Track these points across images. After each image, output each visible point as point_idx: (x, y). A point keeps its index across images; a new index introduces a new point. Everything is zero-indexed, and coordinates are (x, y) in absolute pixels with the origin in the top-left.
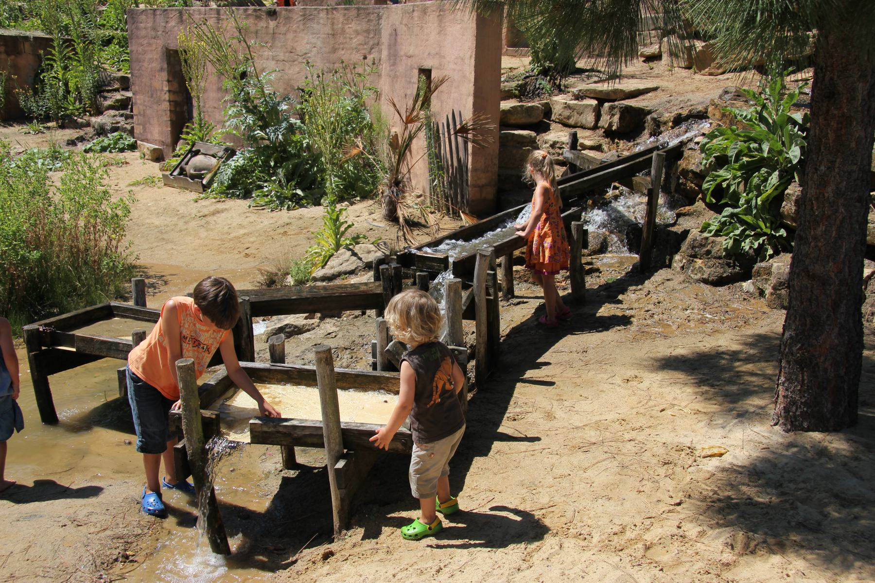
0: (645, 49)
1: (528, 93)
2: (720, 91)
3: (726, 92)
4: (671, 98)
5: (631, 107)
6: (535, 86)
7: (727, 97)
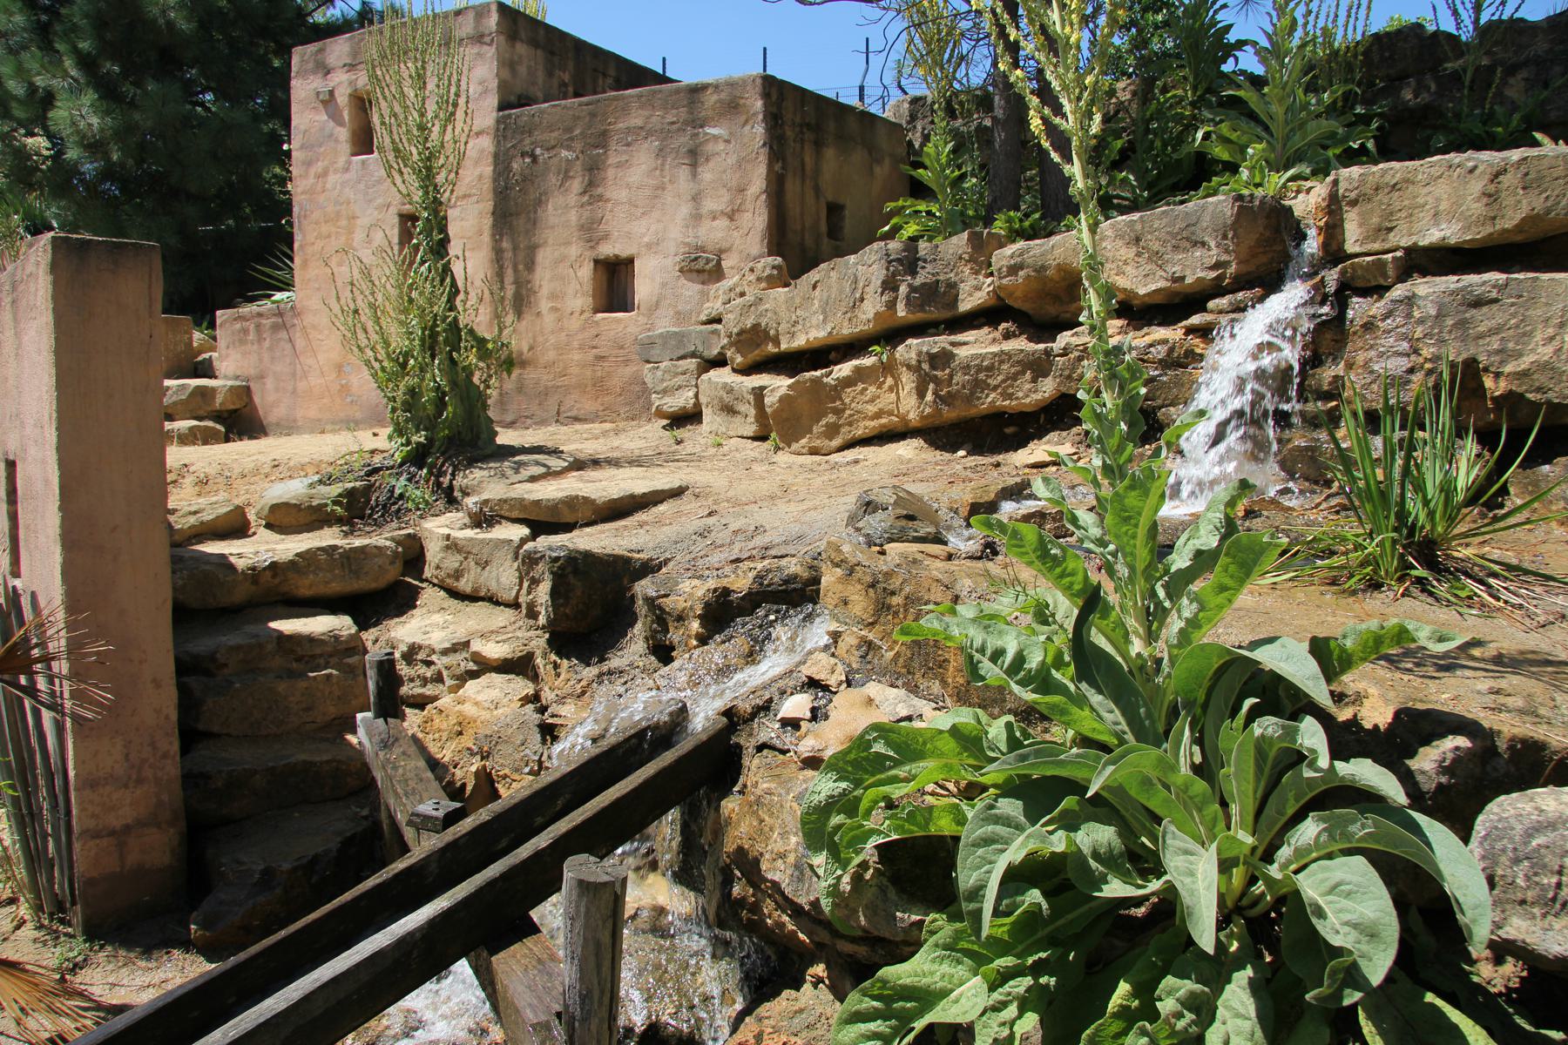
2: (850, 501)
3: (869, 506)
4: (711, 521)
5: (588, 555)
6: (392, 491)
7: (876, 523)
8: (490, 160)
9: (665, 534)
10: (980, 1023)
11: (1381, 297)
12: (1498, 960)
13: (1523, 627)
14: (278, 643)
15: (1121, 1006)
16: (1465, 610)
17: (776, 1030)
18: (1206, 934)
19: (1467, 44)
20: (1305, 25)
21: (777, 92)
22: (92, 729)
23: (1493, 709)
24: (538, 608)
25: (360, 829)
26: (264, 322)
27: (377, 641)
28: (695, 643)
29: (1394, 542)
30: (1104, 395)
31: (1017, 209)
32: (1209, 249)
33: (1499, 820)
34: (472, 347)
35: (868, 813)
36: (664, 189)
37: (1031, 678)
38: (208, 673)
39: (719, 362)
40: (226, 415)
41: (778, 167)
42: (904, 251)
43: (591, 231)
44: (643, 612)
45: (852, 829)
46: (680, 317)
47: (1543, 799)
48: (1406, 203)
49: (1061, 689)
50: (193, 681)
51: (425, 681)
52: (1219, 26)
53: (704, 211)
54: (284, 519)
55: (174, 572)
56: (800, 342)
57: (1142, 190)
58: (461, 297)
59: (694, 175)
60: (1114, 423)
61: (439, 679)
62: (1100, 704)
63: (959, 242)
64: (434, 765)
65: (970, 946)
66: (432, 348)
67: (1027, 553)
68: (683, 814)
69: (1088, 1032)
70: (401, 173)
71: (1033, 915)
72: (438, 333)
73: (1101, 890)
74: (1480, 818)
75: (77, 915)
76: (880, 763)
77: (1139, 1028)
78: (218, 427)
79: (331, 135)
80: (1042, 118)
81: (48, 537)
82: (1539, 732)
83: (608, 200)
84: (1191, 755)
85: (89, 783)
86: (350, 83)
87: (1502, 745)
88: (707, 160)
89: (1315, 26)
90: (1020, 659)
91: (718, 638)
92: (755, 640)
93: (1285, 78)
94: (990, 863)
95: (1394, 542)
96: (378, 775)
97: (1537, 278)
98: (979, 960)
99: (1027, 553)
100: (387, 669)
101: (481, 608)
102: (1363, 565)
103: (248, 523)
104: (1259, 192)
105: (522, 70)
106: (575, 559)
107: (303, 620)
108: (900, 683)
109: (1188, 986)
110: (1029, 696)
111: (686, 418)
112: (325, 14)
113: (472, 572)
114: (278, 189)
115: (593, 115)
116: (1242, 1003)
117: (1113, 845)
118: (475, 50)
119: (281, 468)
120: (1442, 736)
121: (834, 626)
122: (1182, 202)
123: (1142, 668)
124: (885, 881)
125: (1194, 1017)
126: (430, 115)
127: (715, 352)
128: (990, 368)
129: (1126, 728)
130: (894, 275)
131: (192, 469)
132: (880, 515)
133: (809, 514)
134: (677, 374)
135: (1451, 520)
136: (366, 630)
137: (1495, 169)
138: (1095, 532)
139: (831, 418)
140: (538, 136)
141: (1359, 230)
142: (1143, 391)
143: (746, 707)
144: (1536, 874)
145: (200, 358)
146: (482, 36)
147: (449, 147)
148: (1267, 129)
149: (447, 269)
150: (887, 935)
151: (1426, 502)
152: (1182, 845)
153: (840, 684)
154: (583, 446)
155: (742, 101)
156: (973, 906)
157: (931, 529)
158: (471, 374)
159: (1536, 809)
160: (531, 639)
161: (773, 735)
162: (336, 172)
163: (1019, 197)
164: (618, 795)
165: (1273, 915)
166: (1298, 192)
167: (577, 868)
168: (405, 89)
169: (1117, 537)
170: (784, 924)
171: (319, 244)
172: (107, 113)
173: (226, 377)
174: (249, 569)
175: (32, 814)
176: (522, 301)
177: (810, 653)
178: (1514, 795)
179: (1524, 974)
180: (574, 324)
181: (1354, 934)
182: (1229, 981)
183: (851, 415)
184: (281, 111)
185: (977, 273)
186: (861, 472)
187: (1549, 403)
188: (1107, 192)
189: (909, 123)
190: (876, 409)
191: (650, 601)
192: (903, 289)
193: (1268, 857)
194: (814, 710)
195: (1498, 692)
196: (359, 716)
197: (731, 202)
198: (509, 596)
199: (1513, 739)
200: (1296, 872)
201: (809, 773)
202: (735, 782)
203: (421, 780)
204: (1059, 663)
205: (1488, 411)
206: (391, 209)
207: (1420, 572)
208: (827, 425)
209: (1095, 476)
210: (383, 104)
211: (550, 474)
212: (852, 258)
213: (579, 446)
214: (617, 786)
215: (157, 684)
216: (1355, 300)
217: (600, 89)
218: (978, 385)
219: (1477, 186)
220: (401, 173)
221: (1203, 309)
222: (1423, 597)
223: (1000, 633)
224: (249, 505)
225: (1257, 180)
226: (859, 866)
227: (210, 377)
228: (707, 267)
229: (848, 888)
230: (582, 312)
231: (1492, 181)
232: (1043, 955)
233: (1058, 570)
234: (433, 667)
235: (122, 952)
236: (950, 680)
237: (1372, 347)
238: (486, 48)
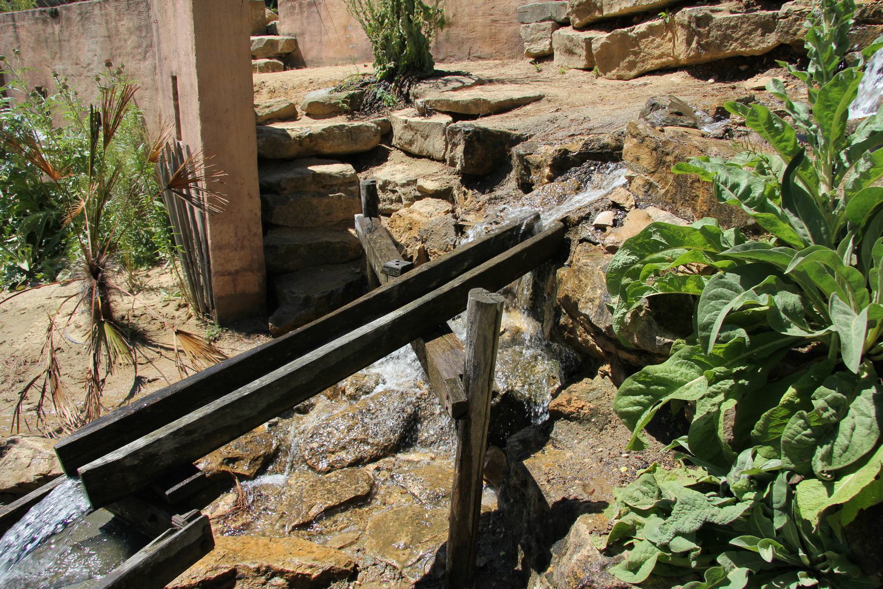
0: (533, 46)
1: (364, 106)
2: (642, 104)
3: (654, 107)
4: (558, 114)
5: (485, 131)
6: (375, 96)
7: (658, 116)
9: (530, 121)
10: (700, 403)
14: (313, 178)
15: (788, 400)
17: (579, 398)
18: (853, 361)
22: (218, 219)
24: (456, 161)
25: (355, 279)
27: (366, 178)
28: (546, 181)
34: (421, 12)
35: (646, 277)
37: (754, 202)
38: (276, 193)
39: (566, 23)
40: (284, 56)
45: (635, 286)
49: (774, 211)
50: (268, 197)
51: (392, 202)
54: (316, 110)
55: (258, 138)
56: (615, 10)
60: (829, 43)
61: (399, 200)
62: (795, 222)
64: (397, 244)
65: (699, 359)
66: (398, 13)
67: (759, 125)
69: (766, 413)
71: (739, 345)
73: (786, 331)
75: (215, 314)
77: (799, 414)
81: (193, 116)
84: (851, 259)
85: (218, 247)
91: (560, 178)
92: (582, 181)
96: (366, 247)
98: (704, 367)
99: (759, 125)
101: (424, 162)
103: (297, 113)
106: (478, 132)
107: (326, 166)
108: (667, 208)
109: (832, 394)
113: (419, 142)
116: (867, 407)
117: (796, 305)
119: (314, 84)
121: (630, 173)
123: (825, 203)
124: (651, 318)
125: (834, 412)
127: (563, 17)
128: (735, 27)
129: (811, 239)
131: (267, 84)
133: (616, 111)
136: (360, 172)
138: (804, 116)
143: (575, 217)
145: (269, 24)
153: (631, 207)
154: (483, 73)
156: (704, 334)
157: (691, 122)
158: (420, 28)
161: (590, 234)
164: (499, 261)
167: (475, 295)
169: (820, 118)
170: (588, 341)
173: (284, 34)
175: (192, 262)
177: (615, 188)
182: (859, 394)
183: (644, 56)
190: (659, 53)
191: (521, 157)
194: (615, 221)
196: (356, 216)
198: (440, 155)
202: (566, 260)
203: (389, 250)
208: (629, 62)
211: (464, 87)
214: (499, 256)
218: (726, 38)
229: (629, 321)
232: (743, 368)
233: (778, 137)
234: (396, 194)
235: (236, 334)
236: (698, 208)
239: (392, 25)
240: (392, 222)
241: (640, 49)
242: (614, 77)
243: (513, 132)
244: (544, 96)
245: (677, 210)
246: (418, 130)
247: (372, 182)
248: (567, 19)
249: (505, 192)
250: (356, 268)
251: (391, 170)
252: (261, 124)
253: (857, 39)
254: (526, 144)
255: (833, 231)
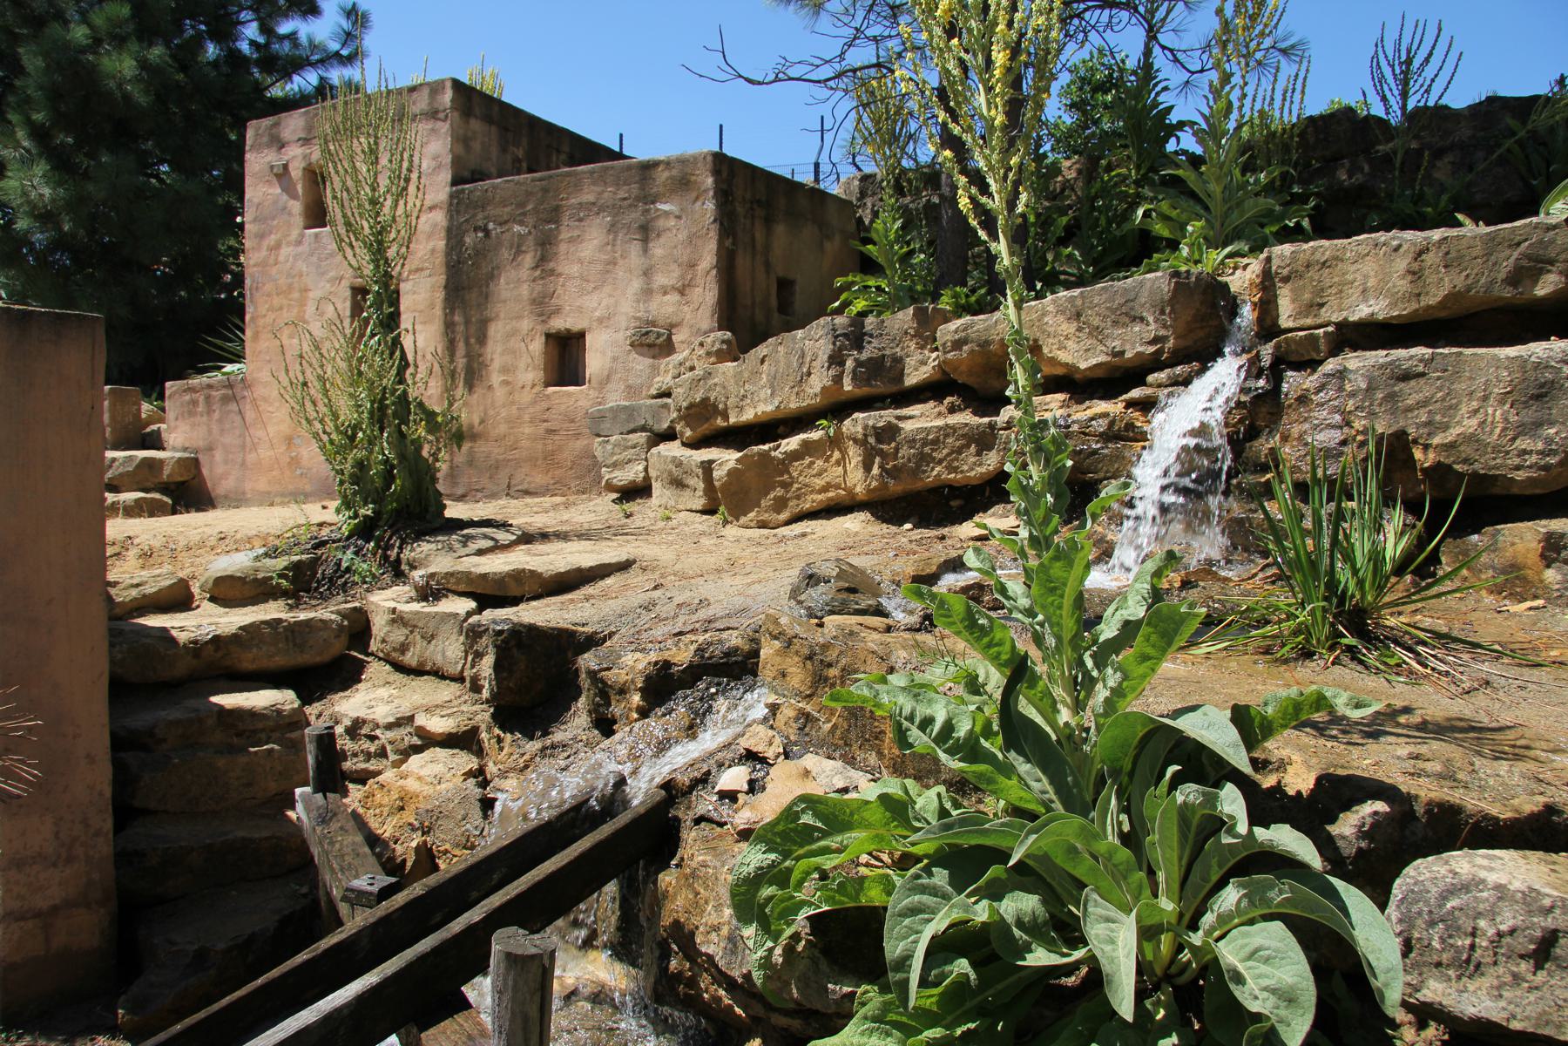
1: (318, 582)
2: (793, 575)
3: (812, 579)
5: (532, 628)
6: (339, 564)
7: (818, 596)
8: (443, 234)
9: (610, 607)
11: (1314, 371)
12: (1421, 1025)
13: (1449, 694)
16: (1392, 677)
19: (1396, 128)
20: (1241, 108)
21: (727, 169)
22: (20, 806)
23: (1413, 774)
24: (482, 682)
26: (214, 393)
28: (635, 716)
29: (1324, 610)
30: (1031, 467)
31: (964, 284)
32: (1148, 324)
33: (1415, 884)
34: (421, 420)
35: (799, 885)
36: (615, 264)
39: (669, 436)
40: (173, 487)
41: (728, 243)
42: (851, 326)
43: (543, 305)
44: (586, 686)
45: (782, 901)
46: (631, 390)
47: (1457, 862)
48: (1336, 279)
49: (989, 758)
51: (369, 756)
52: (1161, 107)
53: (655, 286)
54: (229, 592)
55: (112, 645)
56: (748, 415)
57: (1088, 267)
58: (411, 370)
59: (645, 250)
60: (1040, 495)
61: (382, 753)
62: (1028, 773)
63: (905, 318)
64: (373, 840)
65: (899, 1018)
67: (954, 623)
68: (621, 888)
70: (352, 247)
71: (962, 983)
72: (387, 406)
73: (1025, 959)
74: (1398, 881)
76: (808, 834)
78: (165, 499)
79: (285, 208)
80: (970, 198)
82: (1455, 796)
83: (560, 275)
84: (1120, 824)
86: (305, 157)
87: (1420, 809)
88: (659, 235)
89: (1252, 109)
90: (949, 727)
91: (660, 711)
92: (697, 714)
93: (1222, 158)
94: (917, 932)
95: (1324, 610)
96: (315, 851)
97: (1461, 353)
99: (954, 623)
100: (326, 741)
101: (426, 683)
102: (1296, 633)
104: (1196, 269)
105: (477, 146)
106: (519, 632)
107: (246, 694)
108: (837, 754)
110: (955, 764)
111: (636, 492)
112: (283, 89)
114: (231, 260)
115: (545, 191)
117: (1037, 913)
118: (430, 126)
119: (227, 541)
120: (1362, 801)
121: (772, 699)
122: (1126, 277)
124: (817, 953)
126: (382, 190)
127: (665, 426)
128: (935, 442)
129: (1054, 797)
130: (840, 350)
131: (136, 541)
132: (822, 587)
133: (753, 587)
134: (627, 448)
135: (1380, 589)
136: (310, 704)
137: (1418, 248)
138: (1024, 602)
139: (779, 492)
140: (492, 211)
141: (1292, 306)
142: (1069, 463)
143: (684, 779)
144: (1450, 936)
145: (148, 430)
146: (437, 112)
147: (401, 221)
148: (1207, 209)
149: (396, 342)
150: (818, 1006)
151: (1355, 572)
152: (1103, 912)
153: (777, 757)
154: (532, 520)
155: (693, 178)
156: (899, 976)
158: (420, 447)
159: (1451, 871)
160: (476, 713)
161: (711, 808)
162: (289, 244)
163: (966, 273)
165: (1201, 982)
166: (1235, 268)
167: (504, 941)
168: (358, 164)
169: (1043, 607)
170: (720, 999)
171: (271, 317)
172: (59, 184)
173: (174, 449)
174: (191, 642)
176: (474, 374)
177: (749, 725)
178: (1430, 858)
179: (1446, 1037)
180: (526, 397)
181: (1272, 1000)
183: (799, 489)
184: (236, 183)
185: (922, 347)
186: (808, 546)
187: (1475, 475)
188: (1054, 268)
189: (859, 199)
191: (592, 674)
192: (849, 364)
193: (1194, 927)
194: (751, 783)
195: (1417, 757)
196: (298, 791)
197: (682, 277)
199: (1430, 803)
200: (1217, 940)
201: (744, 845)
202: (673, 855)
203: (358, 855)
204: (987, 732)
205: (1419, 482)
206: (343, 282)
207: (1349, 640)
208: (774, 499)
209: (1022, 547)
210: (336, 179)
211: (498, 547)
212: (800, 333)
213: (528, 520)
214: (553, 859)
215: (91, 759)
216: (1289, 373)
217: (553, 165)
218: (924, 459)
219: (1401, 264)
220: (352, 247)
221: (1141, 382)
222: (1353, 665)
223: (930, 701)
224: (194, 577)
225: (1196, 257)
226: (791, 937)
227: (158, 449)
228: (658, 341)
229: (780, 960)
230: (533, 386)
231: (1416, 259)
232: (972, 1026)
233: (986, 640)
234: (377, 742)
237: (1306, 420)
238: (440, 124)
239: (371, 442)
240: (367, 797)
241: (791, 477)
242: (752, 524)
243: (581, 629)
244: (634, 562)
245: (853, 757)
246: (415, 626)
247: (327, 728)
248: (671, 428)
249: (569, 735)
250: (302, 886)
251: (368, 698)
252: (120, 618)
253: (1110, 460)
254: (602, 650)
255: (1088, 780)
